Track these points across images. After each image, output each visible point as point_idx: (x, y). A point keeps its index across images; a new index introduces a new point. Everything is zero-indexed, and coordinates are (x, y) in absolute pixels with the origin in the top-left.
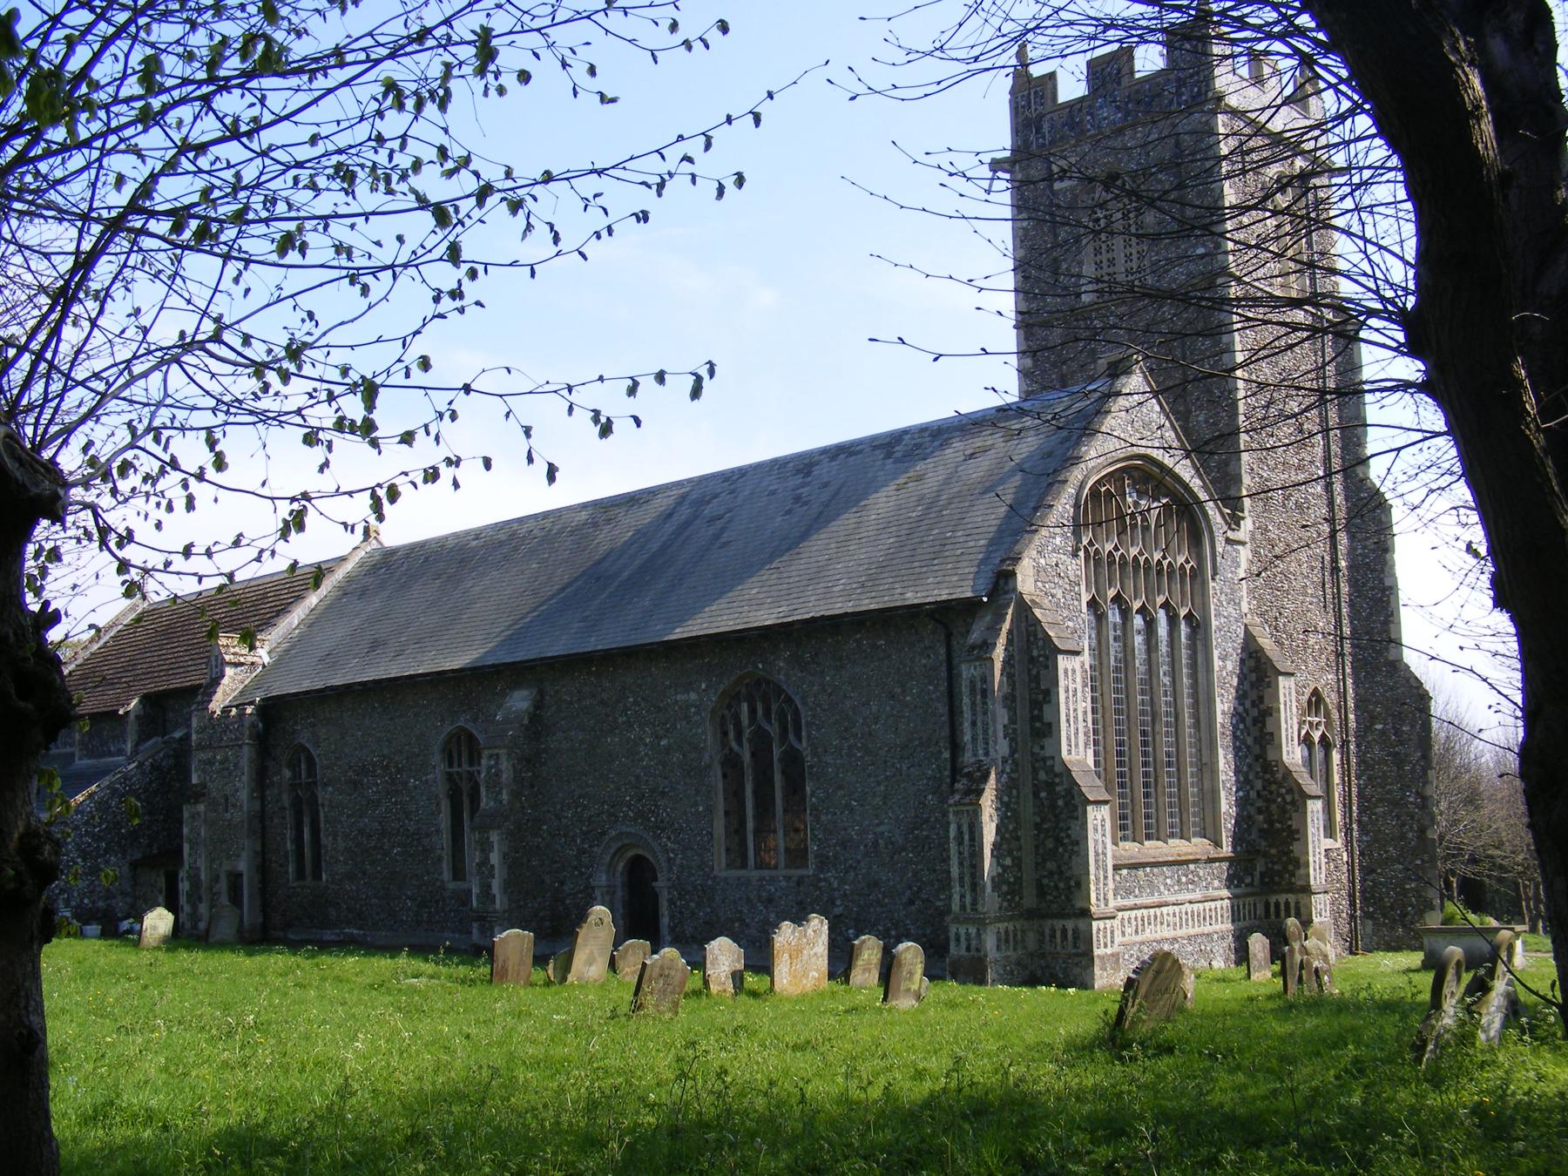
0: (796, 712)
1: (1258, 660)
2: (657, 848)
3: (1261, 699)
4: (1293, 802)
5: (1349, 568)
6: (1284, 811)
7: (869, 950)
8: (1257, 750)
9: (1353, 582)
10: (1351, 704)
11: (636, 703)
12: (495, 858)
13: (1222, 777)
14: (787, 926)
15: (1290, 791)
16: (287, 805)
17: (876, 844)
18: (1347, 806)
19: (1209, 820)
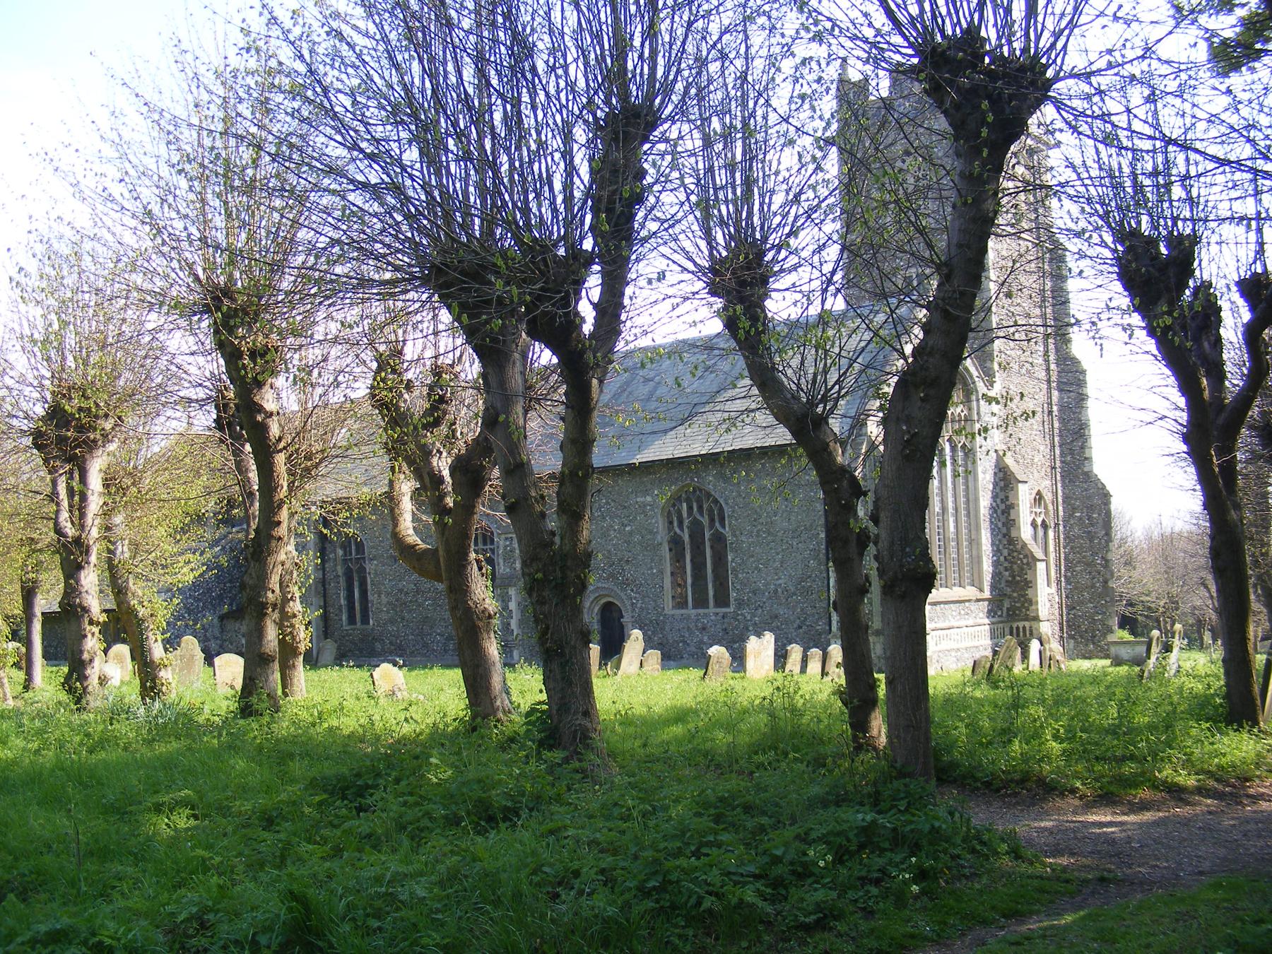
0: (721, 509)
1: (1005, 473)
2: (624, 597)
3: (1007, 497)
4: (1028, 564)
5: (1059, 411)
6: (1022, 569)
7: (795, 652)
8: (1004, 530)
9: (1061, 420)
10: (1060, 500)
11: (607, 503)
12: (513, 605)
13: (984, 548)
14: (753, 639)
15: (1026, 556)
16: (340, 573)
17: (776, 592)
18: (1058, 566)
19: (976, 575)
